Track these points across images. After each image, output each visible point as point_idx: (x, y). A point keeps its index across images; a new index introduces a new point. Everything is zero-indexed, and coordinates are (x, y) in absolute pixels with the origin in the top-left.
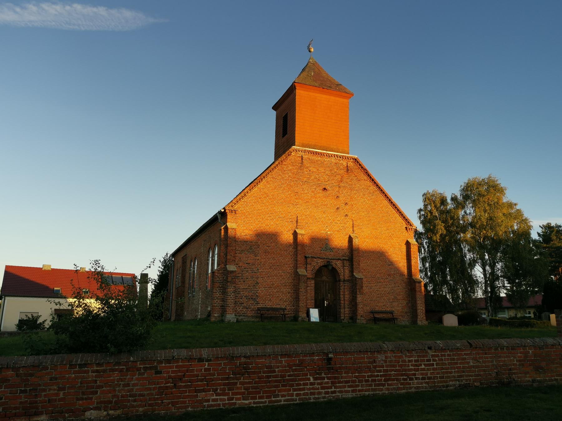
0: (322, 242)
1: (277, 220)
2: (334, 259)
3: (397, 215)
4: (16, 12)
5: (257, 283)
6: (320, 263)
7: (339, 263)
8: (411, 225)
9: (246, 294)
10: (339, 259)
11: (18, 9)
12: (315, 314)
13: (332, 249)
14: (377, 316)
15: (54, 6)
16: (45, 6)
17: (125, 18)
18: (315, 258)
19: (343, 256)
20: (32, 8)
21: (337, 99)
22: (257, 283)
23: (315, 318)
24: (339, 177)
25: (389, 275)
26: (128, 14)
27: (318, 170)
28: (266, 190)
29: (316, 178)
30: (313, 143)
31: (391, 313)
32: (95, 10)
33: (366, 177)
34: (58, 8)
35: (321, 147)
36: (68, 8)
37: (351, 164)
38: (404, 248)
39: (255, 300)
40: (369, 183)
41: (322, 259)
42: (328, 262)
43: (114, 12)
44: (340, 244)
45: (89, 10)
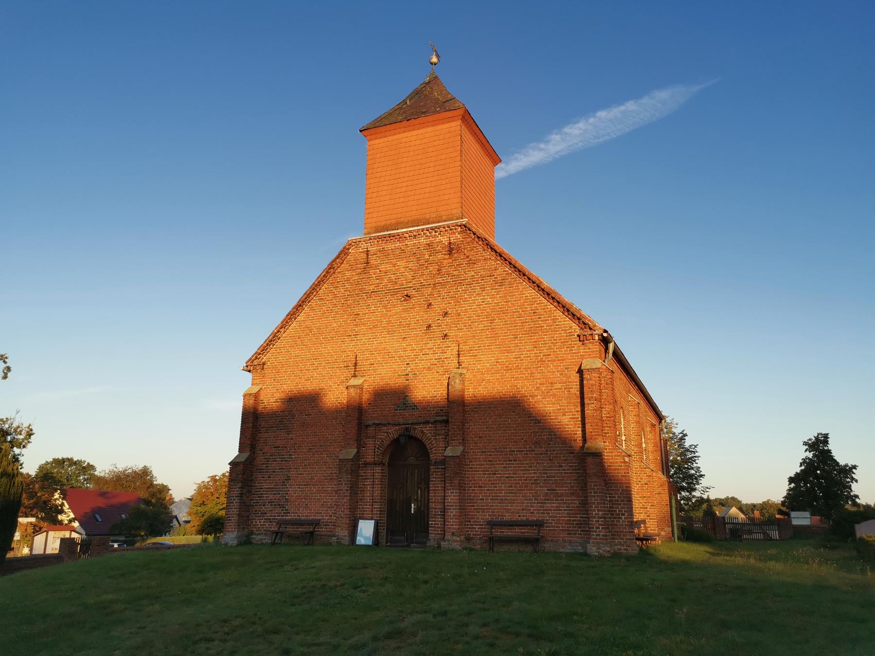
0: (395, 398)
1: (324, 368)
2: (419, 424)
3: (558, 314)
4: (541, 150)
5: (288, 478)
6: (393, 432)
7: (428, 430)
8: (590, 329)
9: (271, 497)
10: (427, 422)
11: (542, 146)
12: (366, 530)
13: (414, 407)
14: (498, 532)
15: (577, 126)
16: (567, 130)
17: (661, 101)
18: (385, 425)
19: (437, 414)
20: (555, 137)
21: (438, 127)
22: (288, 478)
23: (365, 538)
24: (433, 268)
25: (537, 443)
26: (663, 95)
27: (394, 266)
28: (308, 323)
29: (390, 281)
30: (394, 222)
31: (539, 524)
32: (622, 108)
33: (488, 254)
34: (581, 125)
35: (407, 223)
36: (591, 120)
37: (457, 237)
38: (576, 378)
39: (282, 507)
40: (494, 263)
41: (394, 425)
42: (407, 429)
43: (645, 100)
44: (433, 393)
45: (615, 112)
